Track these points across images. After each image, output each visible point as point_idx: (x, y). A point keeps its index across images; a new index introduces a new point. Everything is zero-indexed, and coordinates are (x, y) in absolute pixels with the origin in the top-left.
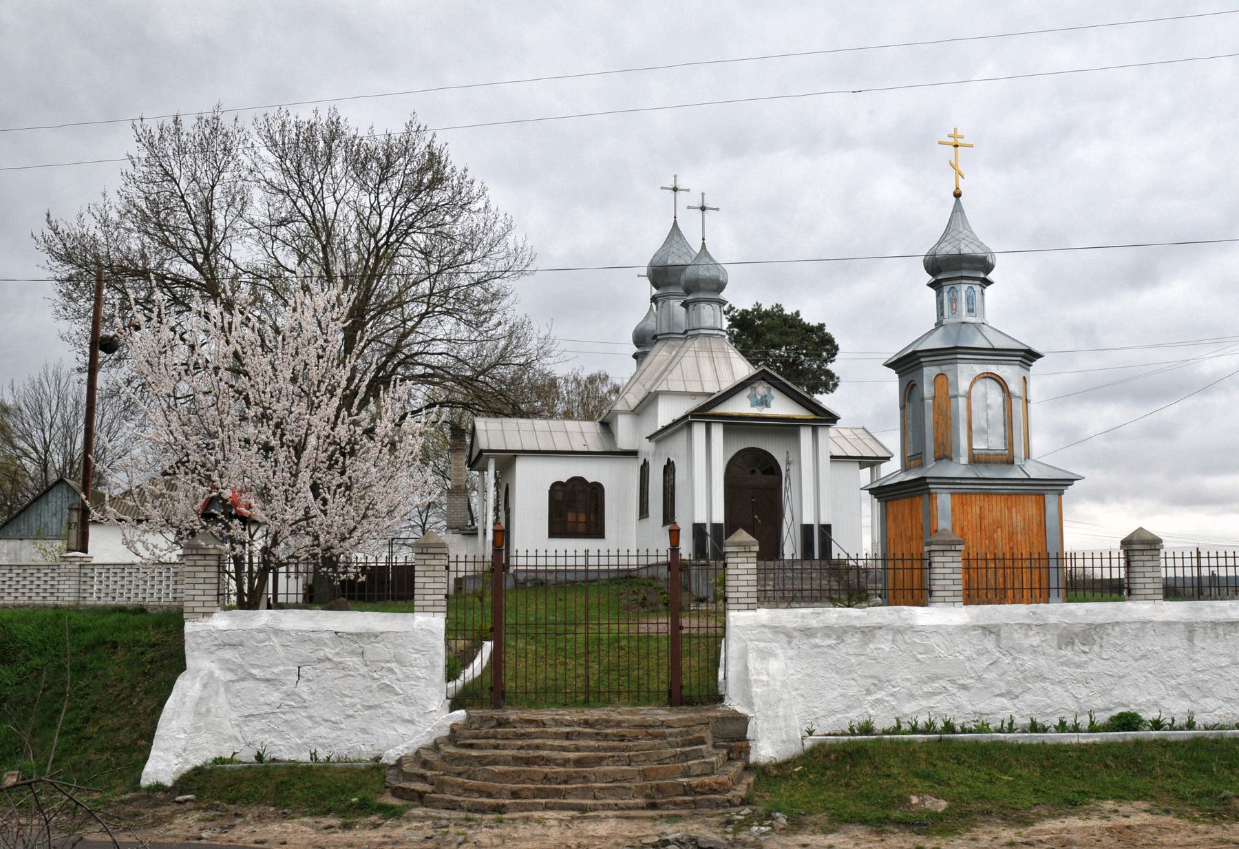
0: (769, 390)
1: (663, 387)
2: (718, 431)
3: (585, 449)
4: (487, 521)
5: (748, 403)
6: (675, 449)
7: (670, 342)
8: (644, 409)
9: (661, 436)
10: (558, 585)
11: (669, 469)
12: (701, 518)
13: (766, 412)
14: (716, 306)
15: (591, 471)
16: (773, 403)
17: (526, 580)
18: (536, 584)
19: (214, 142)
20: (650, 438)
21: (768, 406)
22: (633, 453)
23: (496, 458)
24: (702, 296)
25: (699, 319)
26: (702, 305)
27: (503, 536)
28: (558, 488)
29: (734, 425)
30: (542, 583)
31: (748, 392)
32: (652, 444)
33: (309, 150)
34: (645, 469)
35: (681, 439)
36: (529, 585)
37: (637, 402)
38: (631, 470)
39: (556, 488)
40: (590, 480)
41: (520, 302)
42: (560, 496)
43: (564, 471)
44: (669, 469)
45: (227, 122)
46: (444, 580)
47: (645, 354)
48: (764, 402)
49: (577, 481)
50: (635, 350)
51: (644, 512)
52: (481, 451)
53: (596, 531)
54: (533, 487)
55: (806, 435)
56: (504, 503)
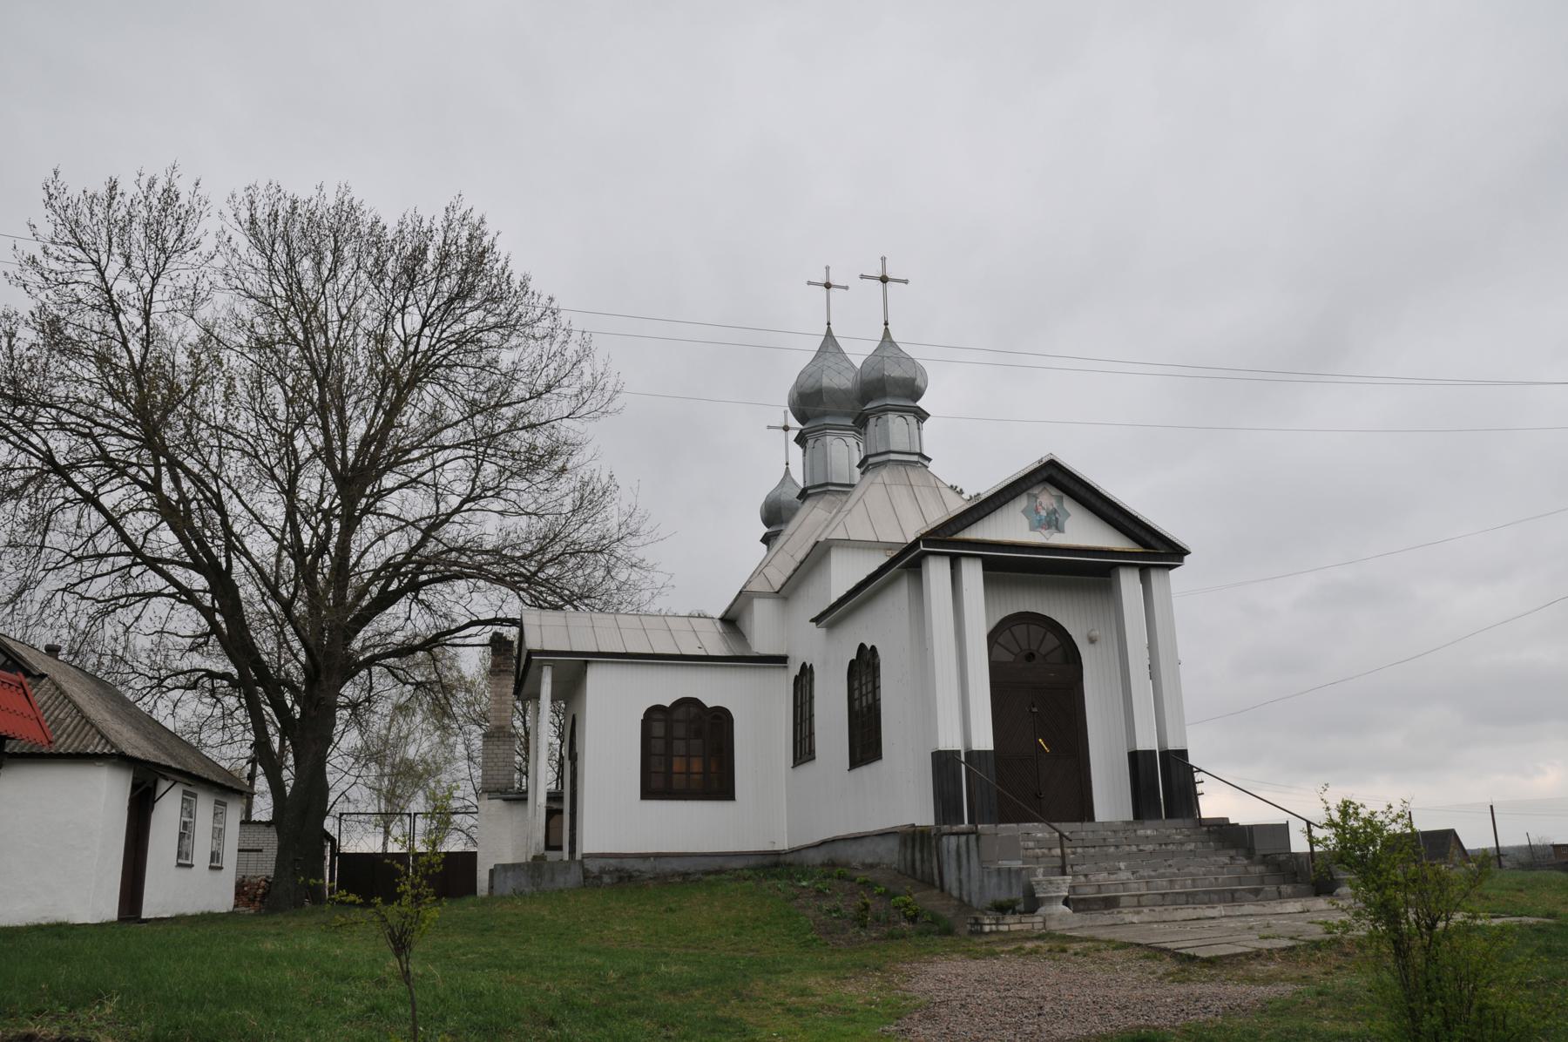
0: (1060, 500)
1: (839, 534)
2: (972, 573)
3: (702, 653)
4: (544, 778)
5: (1025, 522)
6: (882, 627)
7: (828, 497)
8: (796, 588)
9: (832, 617)
10: (663, 879)
11: (865, 667)
12: (950, 741)
13: (1056, 539)
14: (912, 419)
15: (711, 689)
16: (1069, 524)
17: (603, 871)
18: (621, 879)
19: (163, 224)
20: (817, 620)
21: (1060, 529)
22: (781, 660)
23: (555, 667)
24: (889, 401)
25: (886, 437)
26: (891, 416)
27: (562, 809)
28: (659, 716)
29: (1006, 566)
30: (628, 877)
31: (1022, 502)
32: (821, 632)
33: (299, 242)
34: (805, 679)
35: (899, 597)
36: (606, 879)
37: (784, 579)
38: (780, 685)
39: (653, 715)
40: (709, 703)
41: (600, 449)
42: (658, 729)
43: (667, 688)
44: (865, 667)
45: (184, 187)
46: (963, 838)
47: (776, 534)
48: (1053, 522)
49: (689, 704)
50: (766, 530)
51: (803, 751)
52: (530, 653)
53: (716, 782)
54: (615, 712)
55: (1129, 583)
56: (570, 759)
